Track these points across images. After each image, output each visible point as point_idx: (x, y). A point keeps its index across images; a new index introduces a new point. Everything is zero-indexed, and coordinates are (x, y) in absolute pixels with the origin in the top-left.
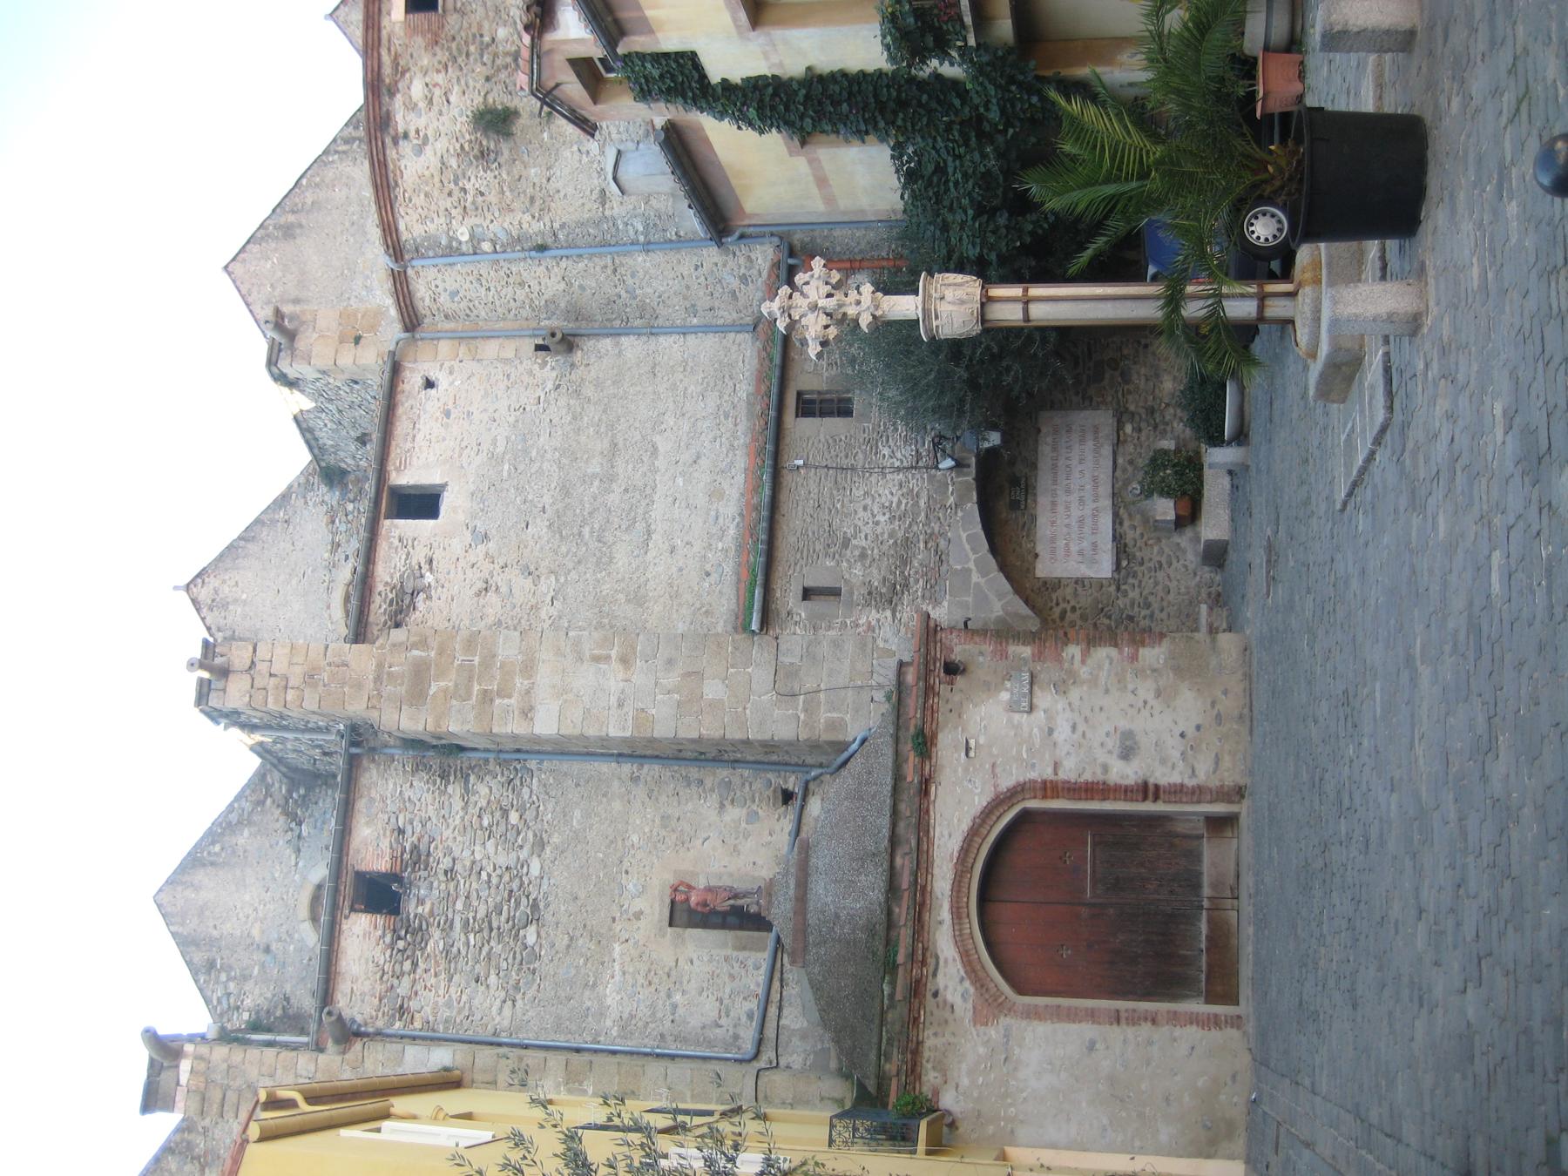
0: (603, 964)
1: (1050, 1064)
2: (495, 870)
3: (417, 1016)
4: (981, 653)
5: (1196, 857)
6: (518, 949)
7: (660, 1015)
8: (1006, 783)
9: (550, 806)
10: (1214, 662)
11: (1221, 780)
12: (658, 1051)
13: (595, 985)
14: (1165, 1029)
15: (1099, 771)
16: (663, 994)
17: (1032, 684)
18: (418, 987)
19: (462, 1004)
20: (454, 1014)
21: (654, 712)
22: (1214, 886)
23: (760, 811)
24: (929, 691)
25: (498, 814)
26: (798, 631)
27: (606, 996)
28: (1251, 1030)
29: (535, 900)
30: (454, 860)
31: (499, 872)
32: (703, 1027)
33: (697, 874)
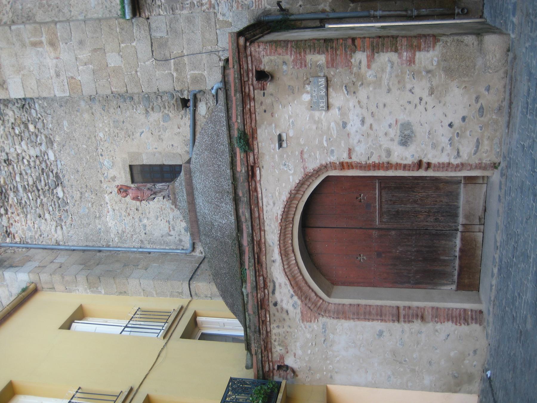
0: (101, 205)
1: (354, 343)
2: (30, 158)
3: (16, 235)
4: (284, 63)
5: (455, 196)
6: (55, 200)
7: (138, 230)
8: (312, 166)
9: (49, 119)
10: (480, 62)
11: (480, 159)
12: (141, 250)
13: (100, 217)
14: (430, 325)
15: (384, 155)
16: (137, 220)
17: (327, 87)
18: (11, 221)
19: (36, 229)
20: (33, 234)
21: (79, 78)
22: (467, 217)
23: (170, 114)
24: (245, 98)
25: (22, 126)
26: (162, 13)
27: (107, 222)
28: (490, 332)
29: (57, 173)
30: (7, 154)
31: (32, 159)
32: (162, 236)
33: (141, 154)
